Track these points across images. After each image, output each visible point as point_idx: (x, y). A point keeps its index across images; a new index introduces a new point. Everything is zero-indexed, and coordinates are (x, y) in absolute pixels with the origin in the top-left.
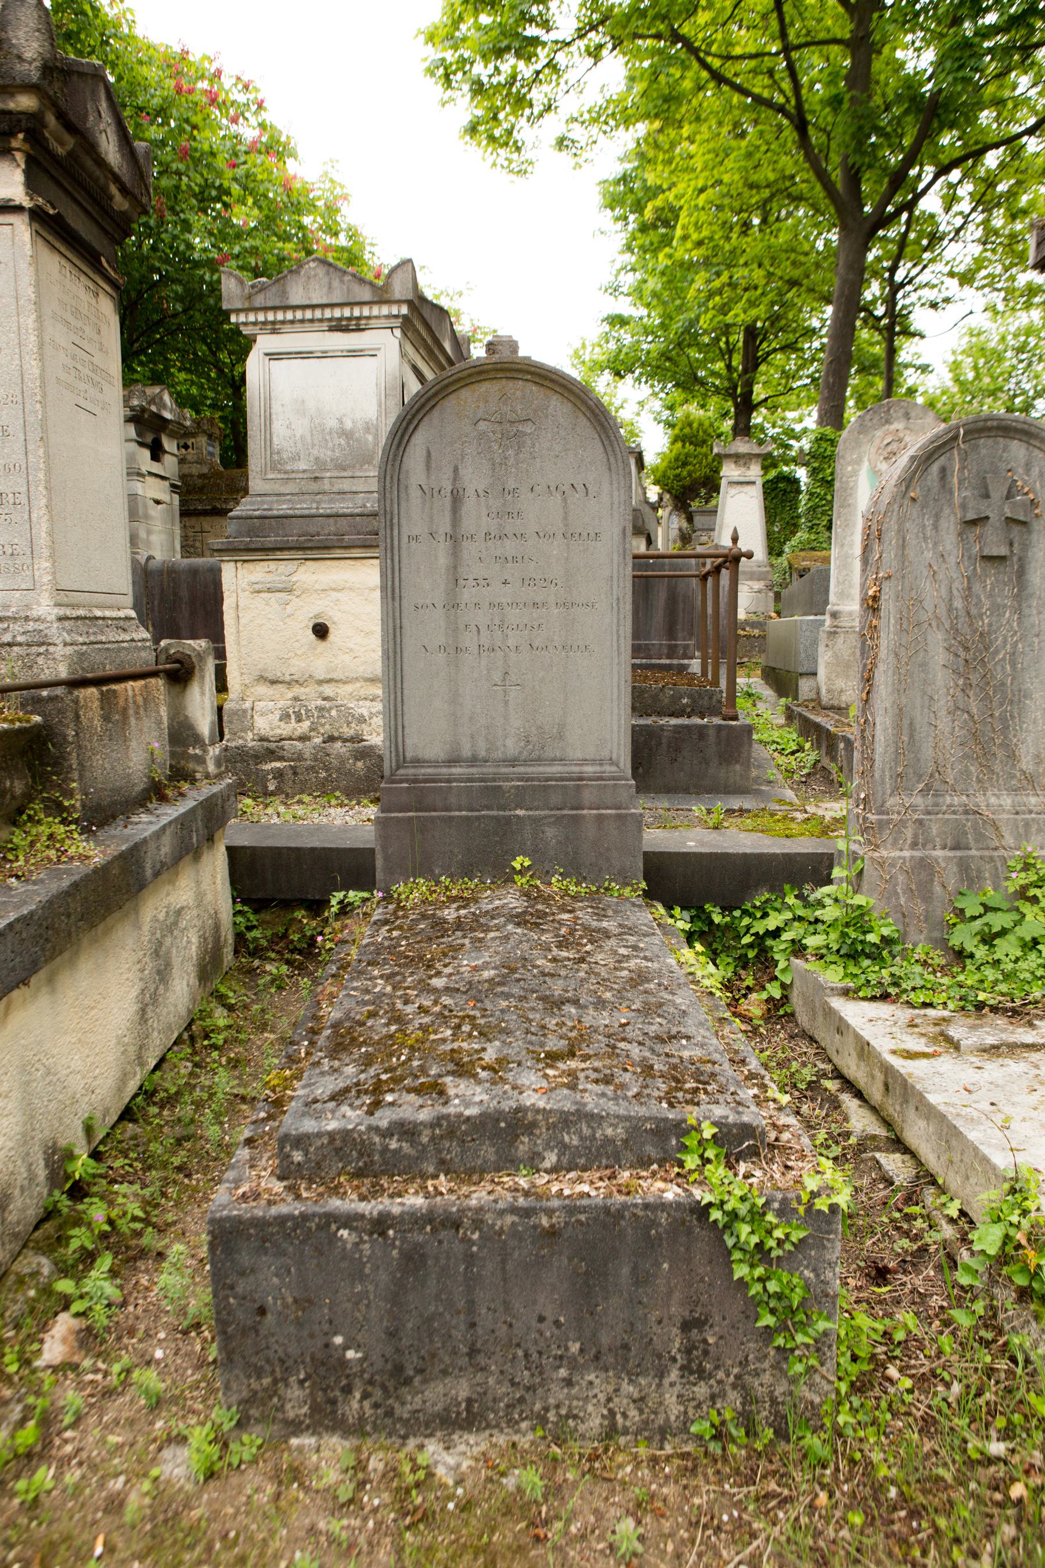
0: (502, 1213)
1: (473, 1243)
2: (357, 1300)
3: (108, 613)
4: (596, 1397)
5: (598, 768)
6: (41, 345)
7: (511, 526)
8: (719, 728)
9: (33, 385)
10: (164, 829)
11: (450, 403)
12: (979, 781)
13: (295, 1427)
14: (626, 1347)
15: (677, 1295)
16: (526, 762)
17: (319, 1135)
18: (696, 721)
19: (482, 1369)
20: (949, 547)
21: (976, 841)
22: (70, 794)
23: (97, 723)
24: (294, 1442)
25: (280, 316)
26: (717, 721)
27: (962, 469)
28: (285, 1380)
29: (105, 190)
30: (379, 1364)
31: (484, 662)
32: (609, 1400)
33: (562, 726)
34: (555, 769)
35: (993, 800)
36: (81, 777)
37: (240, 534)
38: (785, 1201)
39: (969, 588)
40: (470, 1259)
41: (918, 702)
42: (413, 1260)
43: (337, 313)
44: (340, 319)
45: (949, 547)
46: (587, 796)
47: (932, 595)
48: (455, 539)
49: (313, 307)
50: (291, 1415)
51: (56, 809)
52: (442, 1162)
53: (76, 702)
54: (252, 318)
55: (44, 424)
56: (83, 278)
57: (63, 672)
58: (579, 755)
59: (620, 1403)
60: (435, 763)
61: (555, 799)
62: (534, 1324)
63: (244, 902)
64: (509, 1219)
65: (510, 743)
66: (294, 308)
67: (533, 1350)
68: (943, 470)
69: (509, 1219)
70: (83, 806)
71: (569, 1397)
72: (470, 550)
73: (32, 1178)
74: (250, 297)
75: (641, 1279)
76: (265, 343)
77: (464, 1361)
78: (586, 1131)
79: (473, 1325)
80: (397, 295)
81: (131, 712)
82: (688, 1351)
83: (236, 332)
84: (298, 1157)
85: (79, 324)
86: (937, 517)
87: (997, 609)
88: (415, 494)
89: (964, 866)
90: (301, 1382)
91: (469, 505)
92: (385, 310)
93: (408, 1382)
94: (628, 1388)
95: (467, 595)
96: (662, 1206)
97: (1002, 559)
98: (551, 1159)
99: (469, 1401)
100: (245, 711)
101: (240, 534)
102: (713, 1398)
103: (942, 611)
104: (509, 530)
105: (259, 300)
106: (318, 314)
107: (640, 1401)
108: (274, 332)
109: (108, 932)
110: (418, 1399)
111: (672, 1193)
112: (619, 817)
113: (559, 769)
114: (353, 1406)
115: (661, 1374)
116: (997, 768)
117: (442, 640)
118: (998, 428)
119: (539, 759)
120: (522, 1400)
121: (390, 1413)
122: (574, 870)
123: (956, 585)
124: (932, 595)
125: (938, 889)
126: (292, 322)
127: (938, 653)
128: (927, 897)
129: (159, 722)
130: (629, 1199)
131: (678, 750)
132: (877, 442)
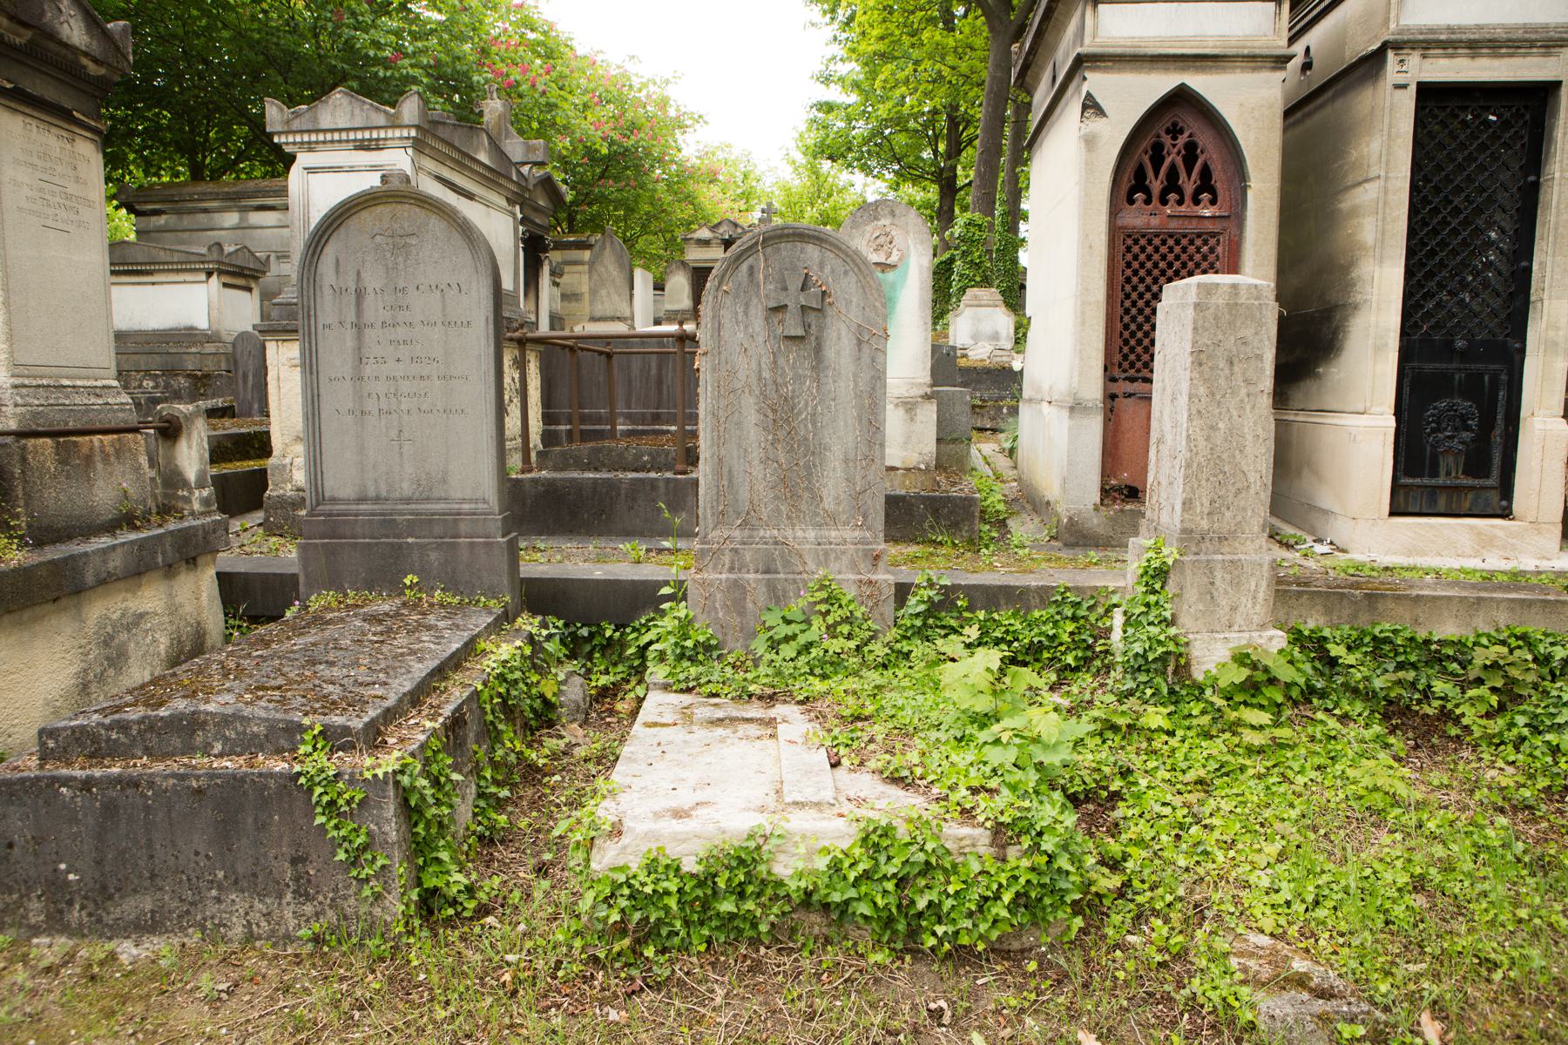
0: (166, 777)
1: (148, 798)
3: (79, 383)
4: (238, 912)
7: (402, 316)
8: (668, 479)
10: (114, 547)
11: (354, 223)
12: (789, 518)
13: (36, 931)
14: (254, 875)
15: (286, 840)
16: (418, 501)
17: (65, 729)
18: (653, 475)
19: (160, 889)
20: (757, 329)
21: (784, 566)
23: (51, 466)
24: (35, 941)
25: (314, 138)
26: (669, 475)
27: (767, 266)
28: (28, 895)
30: (91, 885)
32: (247, 914)
33: (445, 472)
35: (800, 534)
36: (27, 505)
37: (281, 318)
38: (352, 775)
39: (775, 362)
40: (147, 808)
41: (735, 454)
42: (110, 809)
43: (359, 135)
44: (363, 140)
45: (757, 329)
46: (463, 527)
47: (745, 369)
48: (359, 327)
49: (340, 130)
50: (33, 921)
52: (147, 748)
53: (24, 448)
56: (53, 130)
57: (13, 425)
58: (459, 495)
59: (255, 916)
60: (347, 501)
61: (438, 530)
62: (192, 856)
64: (172, 781)
65: (405, 485)
66: (325, 131)
67: (193, 876)
68: (751, 268)
69: (172, 781)
70: (29, 526)
71: (219, 911)
72: (370, 335)
74: (288, 122)
75: (262, 827)
76: (303, 159)
77: (147, 883)
79: (152, 857)
80: (406, 121)
81: (98, 458)
82: (297, 879)
83: (277, 149)
84: (51, 744)
85: (49, 165)
86: (747, 305)
87: (798, 378)
88: (327, 292)
89: (771, 587)
90: (39, 897)
91: (369, 300)
92: (397, 133)
93: (111, 897)
94: (259, 906)
95: (369, 370)
96: (271, 775)
97: (802, 338)
98: (218, 747)
99: (152, 912)
100: (284, 466)
101: (281, 318)
102: (317, 914)
103: (753, 380)
104: (400, 319)
105: (296, 125)
106: (344, 136)
107: (267, 915)
108: (310, 150)
110: (118, 910)
111: (280, 766)
112: (487, 544)
114: (75, 915)
115: (280, 896)
116: (804, 507)
117: (350, 405)
118: (794, 234)
120: (188, 912)
121: (99, 921)
122: (452, 586)
123: (764, 359)
124: (745, 369)
125: (750, 605)
126: (324, 142)
127: (751, 416)
128: (742, 612)
129: (137, 469)
131: (634, 499)
132: (867, 236)
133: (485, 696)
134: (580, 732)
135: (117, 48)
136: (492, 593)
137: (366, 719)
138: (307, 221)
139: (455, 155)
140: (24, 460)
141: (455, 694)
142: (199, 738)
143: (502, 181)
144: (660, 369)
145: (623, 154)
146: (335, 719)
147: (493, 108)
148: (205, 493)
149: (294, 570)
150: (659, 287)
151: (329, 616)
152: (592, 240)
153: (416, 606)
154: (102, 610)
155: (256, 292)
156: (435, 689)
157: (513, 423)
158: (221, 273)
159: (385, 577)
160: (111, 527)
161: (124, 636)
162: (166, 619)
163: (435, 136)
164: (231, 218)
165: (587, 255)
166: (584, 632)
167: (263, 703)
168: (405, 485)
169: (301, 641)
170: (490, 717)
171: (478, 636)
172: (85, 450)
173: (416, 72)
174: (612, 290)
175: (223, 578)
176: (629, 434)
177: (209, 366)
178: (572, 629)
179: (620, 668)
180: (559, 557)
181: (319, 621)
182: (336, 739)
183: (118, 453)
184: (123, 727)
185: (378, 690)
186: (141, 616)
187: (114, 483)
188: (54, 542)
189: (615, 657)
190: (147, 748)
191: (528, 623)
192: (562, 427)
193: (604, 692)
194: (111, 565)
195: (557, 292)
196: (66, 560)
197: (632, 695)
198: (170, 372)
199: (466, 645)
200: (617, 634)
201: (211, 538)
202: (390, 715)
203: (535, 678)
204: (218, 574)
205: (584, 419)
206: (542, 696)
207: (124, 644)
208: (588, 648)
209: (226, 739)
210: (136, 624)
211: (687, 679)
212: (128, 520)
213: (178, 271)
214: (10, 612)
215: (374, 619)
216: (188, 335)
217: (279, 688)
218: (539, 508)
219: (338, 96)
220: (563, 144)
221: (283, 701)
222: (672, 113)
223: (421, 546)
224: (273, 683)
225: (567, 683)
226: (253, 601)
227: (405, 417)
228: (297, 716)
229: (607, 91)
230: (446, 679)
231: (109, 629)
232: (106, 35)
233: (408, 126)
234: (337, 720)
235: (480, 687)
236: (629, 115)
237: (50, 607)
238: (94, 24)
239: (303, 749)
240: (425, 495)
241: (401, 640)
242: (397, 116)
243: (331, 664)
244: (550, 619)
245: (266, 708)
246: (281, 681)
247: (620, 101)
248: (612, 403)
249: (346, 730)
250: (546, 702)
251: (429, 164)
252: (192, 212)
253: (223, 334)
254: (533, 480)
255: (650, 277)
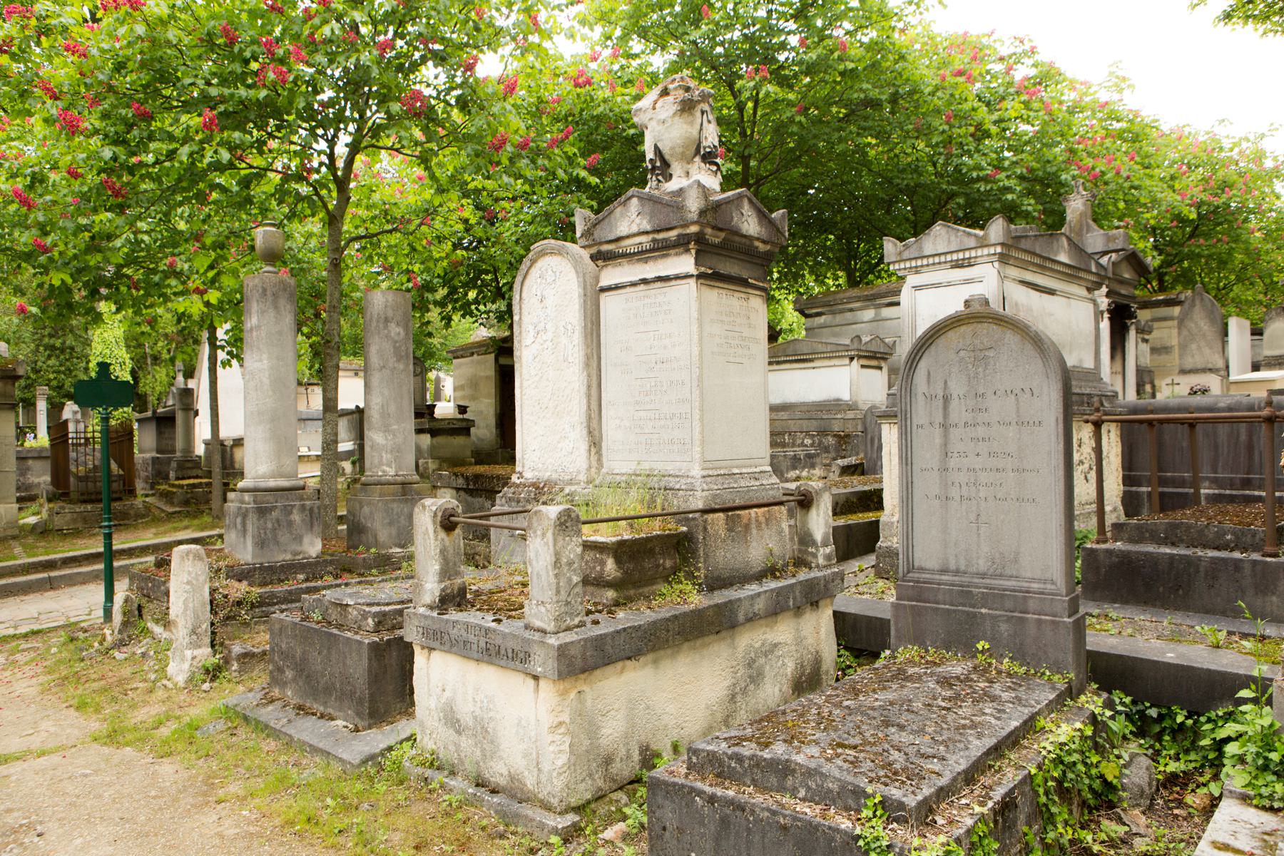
0: (763, 809)
2: (702, 836)
3: (744, 470)
5: (1042, 586)
6: (701, 339)
7: (981, 417)
8: (1255, 562)
9: (695, 359)
10: (759, 594)
11: (942, 342)
17: (703, 751)
18: (1237, 555)
22: (698, 569)
23: (722, 533)
25: (919, 263)
26: (1256, 556)
29: (752, 246)
31: (964, 507)
33: (1017, 553)
34: (1011, 583)
40: (749, 830)
43: (955, 257)
46: (1032, 605)
48: (945, 426)
51: (690, 576)
53: (706, 521)
54: (902, 266)
55: (700, 379)
56: (737, 294)
57: (700, 505)
58: (1029, 575)
60: (932, 572)
61: (1009, 604)
63: (846, 648)
65: (981, 562)
69: (767, 814)
70: (706, 577)
72: (955, 433)
73: (629, 757)
76: (912, 280)
78: (819, 782)
81: (753, 526)
88: (921, 398)
91: (954, 404)
92: (986, 251)
95: (952, 463)
96: (838, 830)
98: (802, 793)
104: (979, 420)
105: (906, 255)
106: (943, 259)
108: (917, 273)
109: (704, 646)
111: (845, 824)
112: (1053, 622)
113: (1014, 583)
117: (937, 492)
119: (1001, 575)
129: (780, 532)
130: (823, 821)
133: (1039, 780)
134: (1143, 820)
135: (778, 230)
136: (1057, 668)
137: (920, 798)
138: (914, 328)
139: (1037, 260)
140: (705, 529)
141: (1007, 779)
142: (789, 782)
143: (1082, 274)
144: (1250, 435)
145: (1214, 212)
146: (894, 791)
147: (1076, 206)
148: (828, 550)
149: (887, 615)
150: (1257, 332)
151: (911, 671)
152: (1182, 297)
153: (983, 671)
154: (749, 639)
155: (885, 370)
156: (990, 767)
157: (1084, 490)
158: (860, 357)
159: (960, 637)
160: (759, 577)
161: (762, 661)
162: (793, 648)
163: (1018, 249)
164: (869, 314)
165: (1176, 310)
166: (1153, 712)
167: (839, 762)
168: (981, 562)
169: (881, 696)
170: (1043, 799)
171: (1038, 713)
172: (745, 521)
173: (1012, 183)
174: (1203, 344)
175: (836, 614)
176: (1215, 499)
177: (850, 428)
178: (1140, 707)
179: (1193, 756)
180: (1130, 631)
181: (901, 675)
182: (892, 811)
183: (767, 520)
184: (739, 758)
185: (935, 765)
186: (776, 645)
187: (766, 542)
188: (720, 588)
189: (1187, 744)
190: (753, 780)
191: (1092, 702)
192: (1144, 489)
193: (1172, 780)
194: (756, 607)
195: (1145, 348)
196: (726, 604)
197: (1203, 791)
198: (823, 433)
199: (1025, 722)
200: (1190, 722)
201: (831, 586)
202: (943, 794)
203: (1095, 759)
204: (835, 613)
205: (1163, 482)
206: (1102, 776)
207: (762, 666)
208: (1157, 729)
209: (809, 788)
210: (772, 651)
211: (1271, 797)
212: (771, 571)
213: (830, 358)
214: (687, 640)
215: (945, 682)
216: (835, 406)
217: (855, 747)
218: (1115, 577)
219: (938, 228)
220: (1150, 217)
221: (855, 763)
222: (1269, 164)
223: (994, 617)
224: (852, 741)
225: (1133, 765)
226: (861, 639)
227: (983, 503)
228: (862, 782)
229: (1195, 157)
230: (1002, 756)
231: (752, 655)
232: (771, 223)
233: (994, 245)
234: (895, 793)
235: (1033, 771)
236: (1221, 174)
237: (713, 637)
238: (763, 217)
239: (866, 813)
240: (998, 572)
241: (966, 710)
242: (985, 237)
243: (902, 728)
244: (1117, 696)
245: (840, 768)
246: (857, 740)
247: (1214, 166)
248: (1195, 468)
249: (901, 806)
250: (1107, 785)
251: (1014, 272)
252: (842, 312)
253: (860, 403)
254: (1107, 551)
255: (1248, 323)
